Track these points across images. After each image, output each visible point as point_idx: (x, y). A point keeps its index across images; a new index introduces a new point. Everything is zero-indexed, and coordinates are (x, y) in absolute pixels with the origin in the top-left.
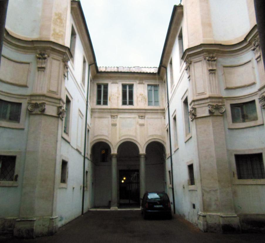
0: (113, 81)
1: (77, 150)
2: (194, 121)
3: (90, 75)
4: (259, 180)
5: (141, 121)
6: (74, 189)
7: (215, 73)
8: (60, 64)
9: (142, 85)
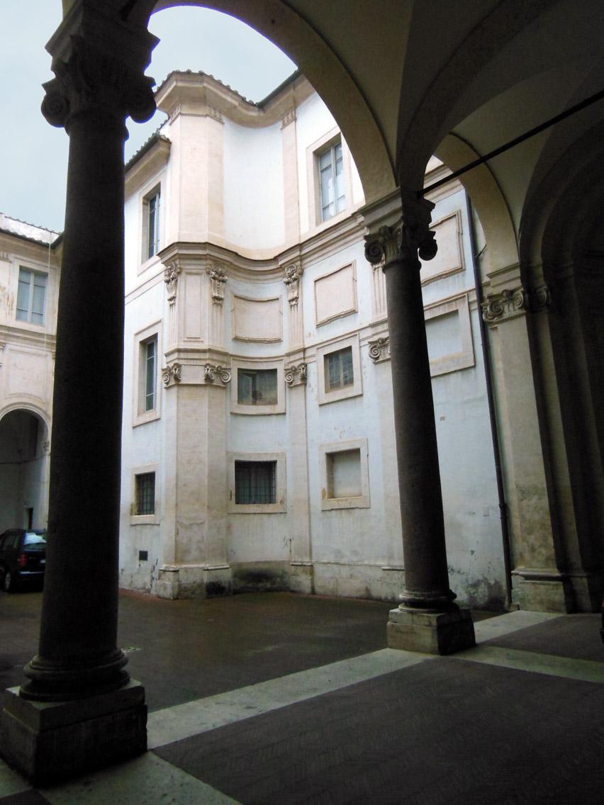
7: (221, 305)
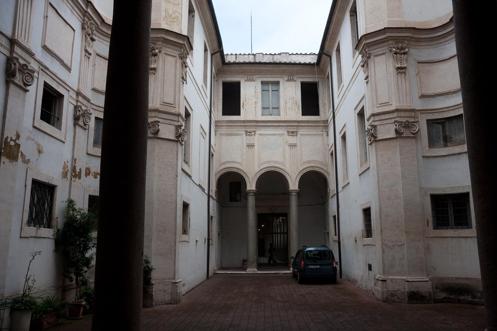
1: (200, 186)
2: (374, 144)
3: (213, 70)
4: (462, 230)
7: (405, 73)
8: (176, 62)
9: (292, 83)
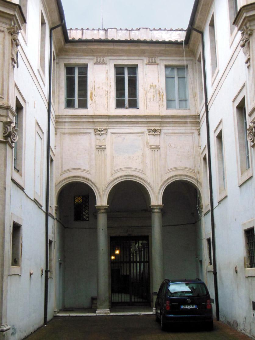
0: (97, 59)
1: (35, 201)
3: (53, 49)
5: (153, 140)
6: (32, 276)
9: (153, 68)
